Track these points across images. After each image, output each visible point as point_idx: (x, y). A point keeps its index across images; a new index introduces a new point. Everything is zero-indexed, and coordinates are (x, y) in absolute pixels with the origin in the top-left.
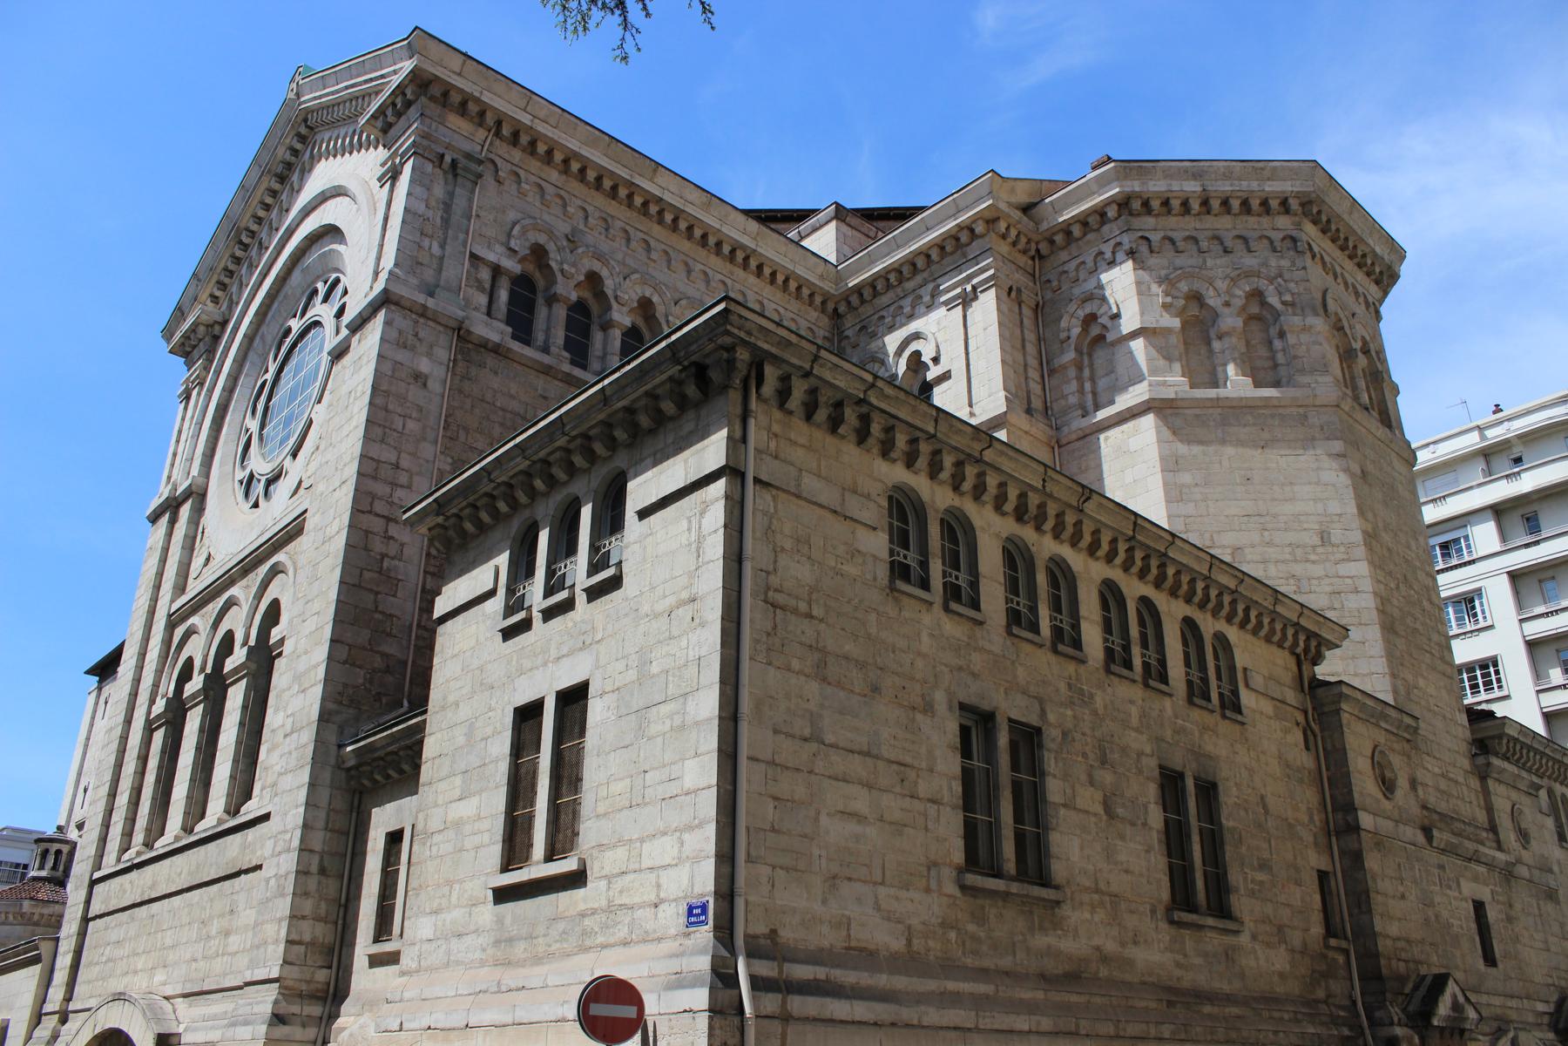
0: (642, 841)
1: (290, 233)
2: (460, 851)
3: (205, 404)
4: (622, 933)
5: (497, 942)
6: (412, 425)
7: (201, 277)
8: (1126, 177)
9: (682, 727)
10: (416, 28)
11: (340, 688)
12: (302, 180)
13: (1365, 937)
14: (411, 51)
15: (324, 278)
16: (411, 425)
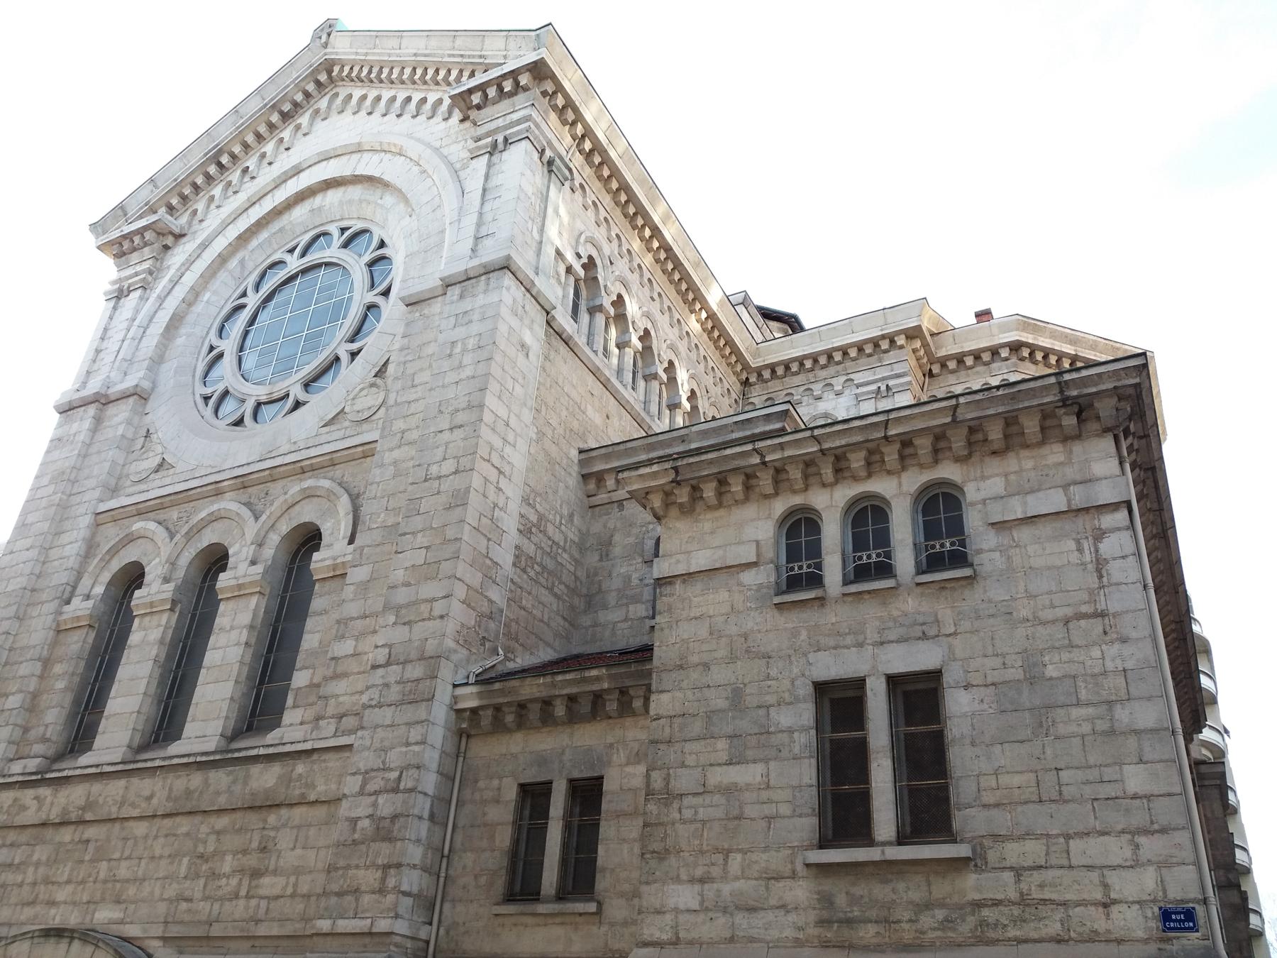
0: (1068, 837)
1: (297, 171)
2: (739, 818)
3: (153, 309)
4: (1054, 928)
5: (821, 922)
6: (518, 388)
7: (159, 184)
8: (1023, 330)
9: (1111, 732)
10: (550, 24)
11: (459, 628)
12: (311, 125)
13: (1113, 904)
14: (538, 43)
15: (344, 224)
16: (518, 388)
